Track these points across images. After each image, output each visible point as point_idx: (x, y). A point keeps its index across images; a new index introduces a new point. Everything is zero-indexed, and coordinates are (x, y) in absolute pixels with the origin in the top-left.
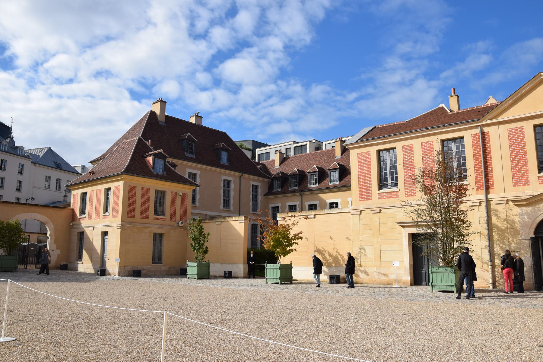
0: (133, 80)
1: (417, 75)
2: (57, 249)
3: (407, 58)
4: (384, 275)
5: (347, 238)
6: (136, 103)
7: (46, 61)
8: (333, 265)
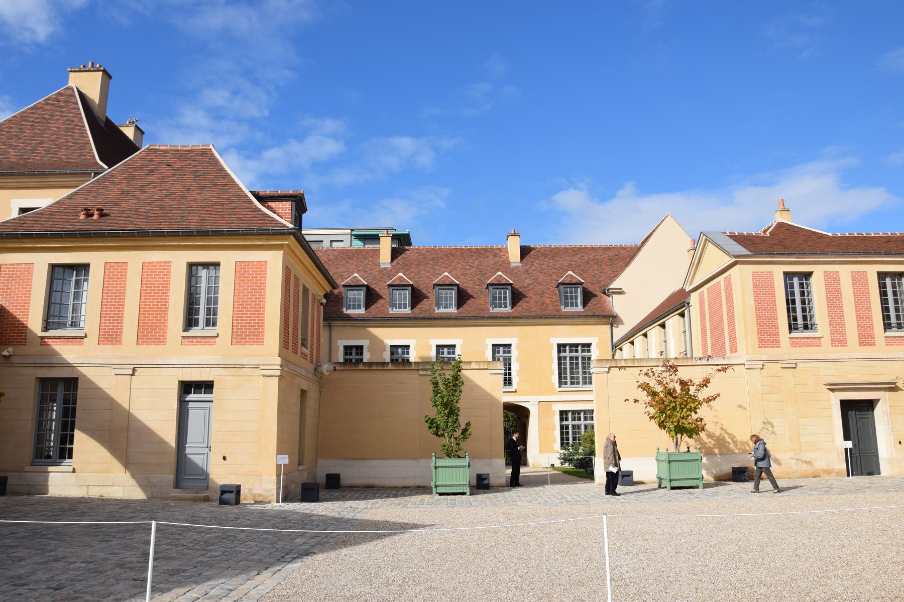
1: (230, 146)
3: (217, 114)
4: (806, 462)
5: (740, 406)
8: (716, 451)
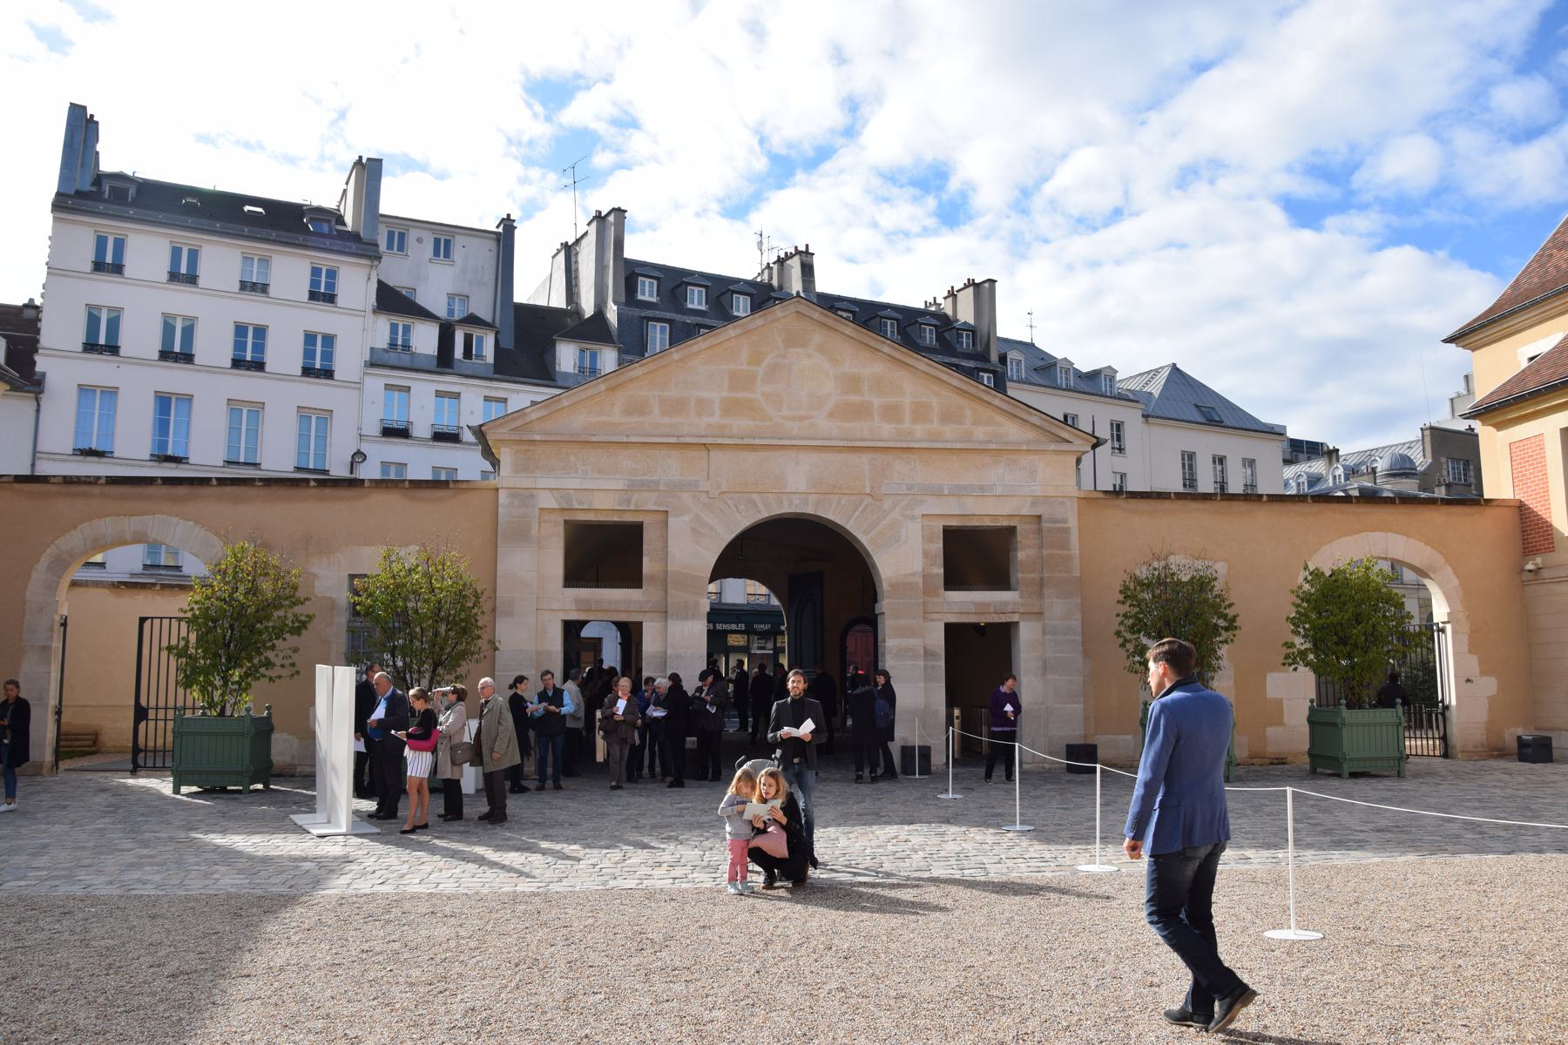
0: (1289, 169)
2: (1484, 673)
6: (1307, 236)
7: (1045, 179)
